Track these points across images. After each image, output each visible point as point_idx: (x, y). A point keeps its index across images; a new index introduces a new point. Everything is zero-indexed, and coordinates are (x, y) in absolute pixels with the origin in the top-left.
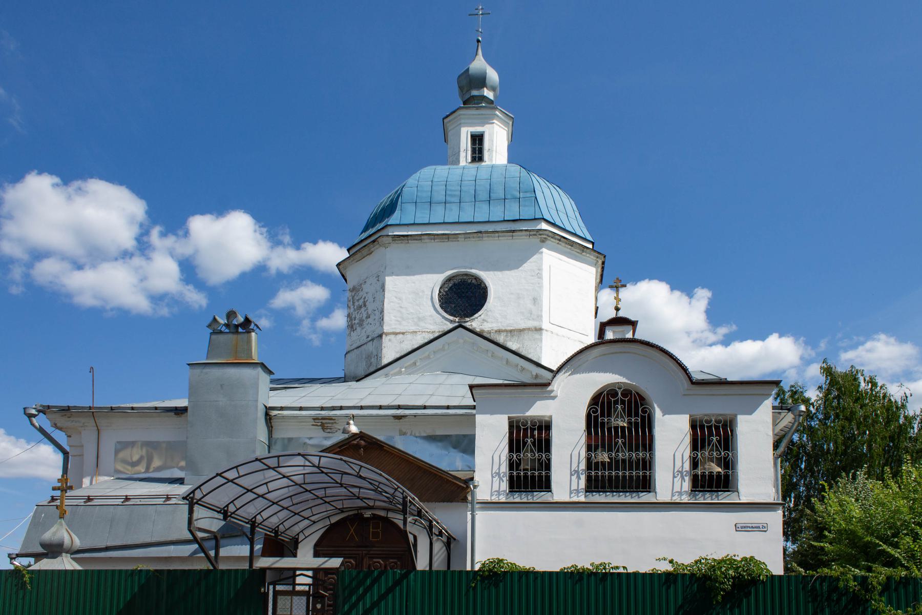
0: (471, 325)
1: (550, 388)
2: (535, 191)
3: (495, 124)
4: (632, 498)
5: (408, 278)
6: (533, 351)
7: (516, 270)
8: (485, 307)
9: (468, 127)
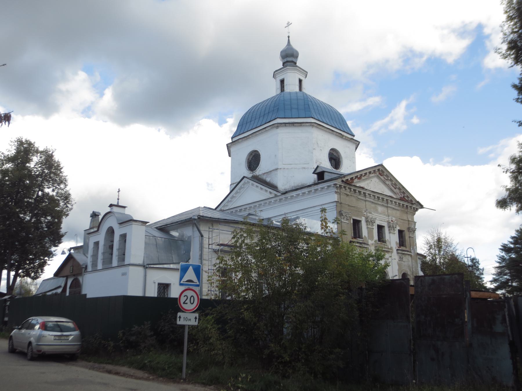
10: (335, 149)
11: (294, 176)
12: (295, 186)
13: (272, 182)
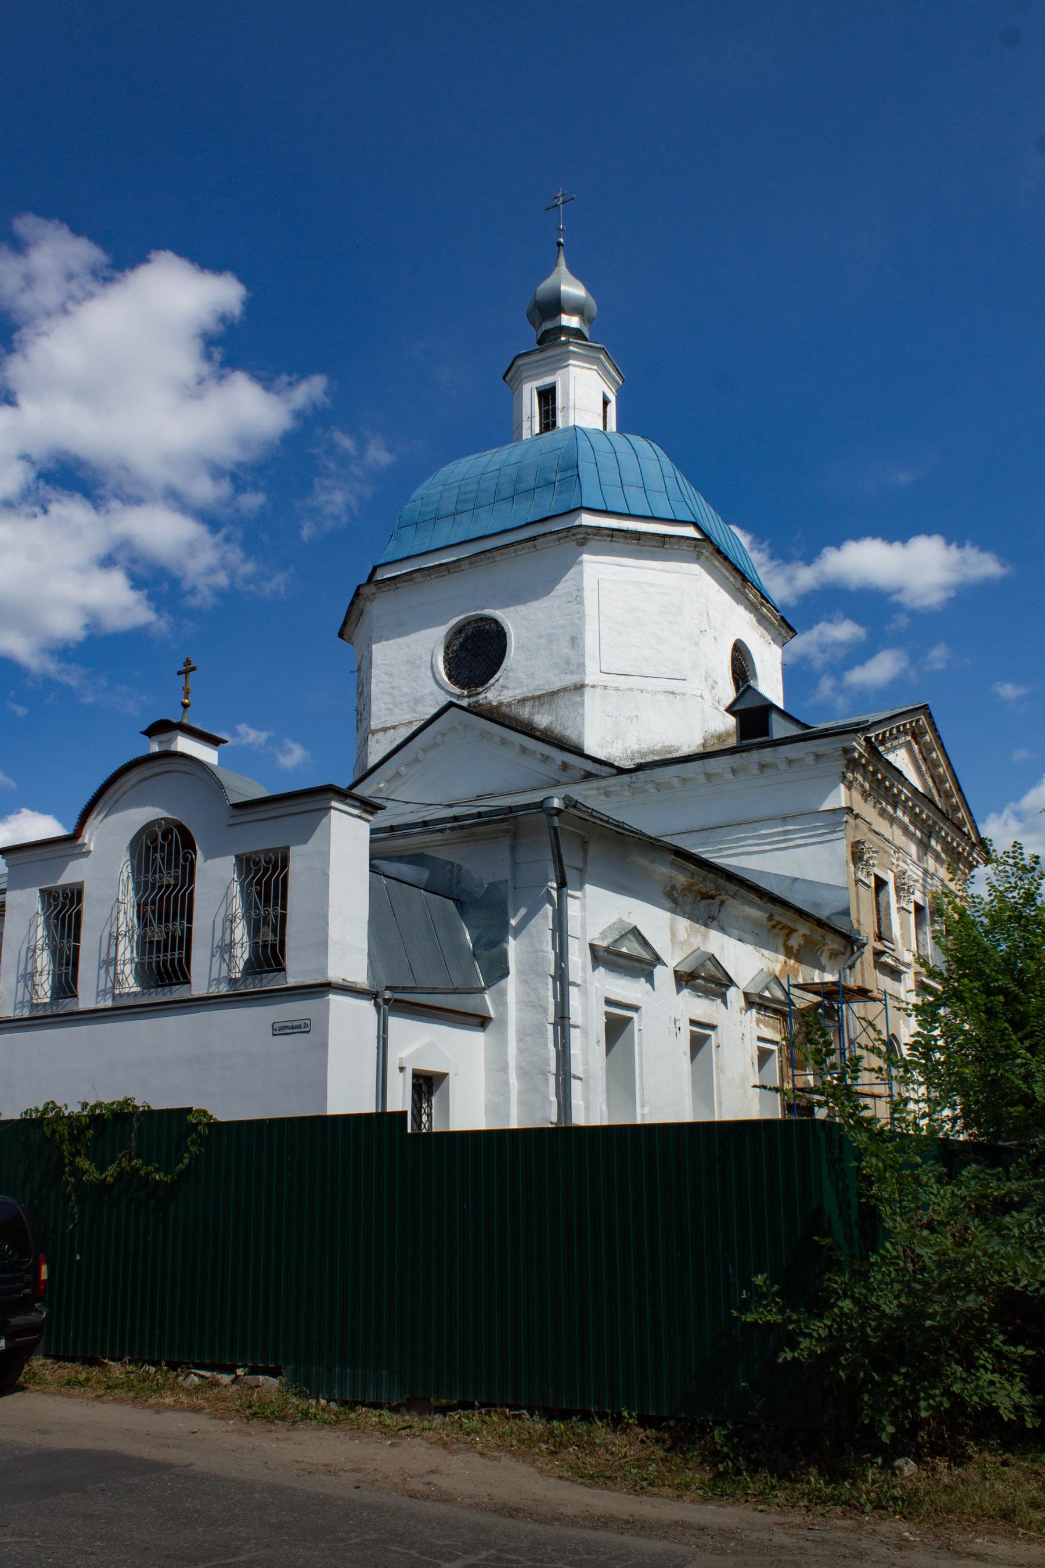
0: (486, 697)
1: (80, 841)
2: (577, 467)
3: (571, 367)
4: (164, 995)
5: (400, 640)
6: (571, 724)
7: (545, 598)
8: (503, 666)
9: (532, 381)
10: (749, 652)
11: (637, 717)
12: (643, 751)
13: (558, 729)
